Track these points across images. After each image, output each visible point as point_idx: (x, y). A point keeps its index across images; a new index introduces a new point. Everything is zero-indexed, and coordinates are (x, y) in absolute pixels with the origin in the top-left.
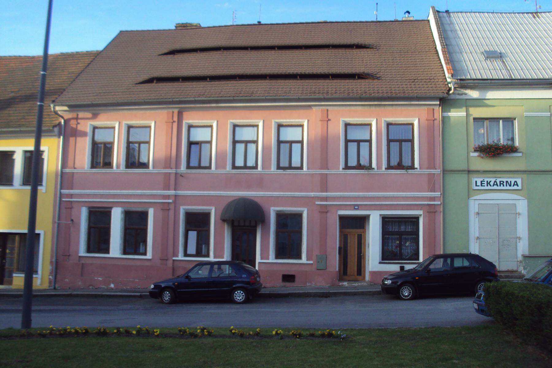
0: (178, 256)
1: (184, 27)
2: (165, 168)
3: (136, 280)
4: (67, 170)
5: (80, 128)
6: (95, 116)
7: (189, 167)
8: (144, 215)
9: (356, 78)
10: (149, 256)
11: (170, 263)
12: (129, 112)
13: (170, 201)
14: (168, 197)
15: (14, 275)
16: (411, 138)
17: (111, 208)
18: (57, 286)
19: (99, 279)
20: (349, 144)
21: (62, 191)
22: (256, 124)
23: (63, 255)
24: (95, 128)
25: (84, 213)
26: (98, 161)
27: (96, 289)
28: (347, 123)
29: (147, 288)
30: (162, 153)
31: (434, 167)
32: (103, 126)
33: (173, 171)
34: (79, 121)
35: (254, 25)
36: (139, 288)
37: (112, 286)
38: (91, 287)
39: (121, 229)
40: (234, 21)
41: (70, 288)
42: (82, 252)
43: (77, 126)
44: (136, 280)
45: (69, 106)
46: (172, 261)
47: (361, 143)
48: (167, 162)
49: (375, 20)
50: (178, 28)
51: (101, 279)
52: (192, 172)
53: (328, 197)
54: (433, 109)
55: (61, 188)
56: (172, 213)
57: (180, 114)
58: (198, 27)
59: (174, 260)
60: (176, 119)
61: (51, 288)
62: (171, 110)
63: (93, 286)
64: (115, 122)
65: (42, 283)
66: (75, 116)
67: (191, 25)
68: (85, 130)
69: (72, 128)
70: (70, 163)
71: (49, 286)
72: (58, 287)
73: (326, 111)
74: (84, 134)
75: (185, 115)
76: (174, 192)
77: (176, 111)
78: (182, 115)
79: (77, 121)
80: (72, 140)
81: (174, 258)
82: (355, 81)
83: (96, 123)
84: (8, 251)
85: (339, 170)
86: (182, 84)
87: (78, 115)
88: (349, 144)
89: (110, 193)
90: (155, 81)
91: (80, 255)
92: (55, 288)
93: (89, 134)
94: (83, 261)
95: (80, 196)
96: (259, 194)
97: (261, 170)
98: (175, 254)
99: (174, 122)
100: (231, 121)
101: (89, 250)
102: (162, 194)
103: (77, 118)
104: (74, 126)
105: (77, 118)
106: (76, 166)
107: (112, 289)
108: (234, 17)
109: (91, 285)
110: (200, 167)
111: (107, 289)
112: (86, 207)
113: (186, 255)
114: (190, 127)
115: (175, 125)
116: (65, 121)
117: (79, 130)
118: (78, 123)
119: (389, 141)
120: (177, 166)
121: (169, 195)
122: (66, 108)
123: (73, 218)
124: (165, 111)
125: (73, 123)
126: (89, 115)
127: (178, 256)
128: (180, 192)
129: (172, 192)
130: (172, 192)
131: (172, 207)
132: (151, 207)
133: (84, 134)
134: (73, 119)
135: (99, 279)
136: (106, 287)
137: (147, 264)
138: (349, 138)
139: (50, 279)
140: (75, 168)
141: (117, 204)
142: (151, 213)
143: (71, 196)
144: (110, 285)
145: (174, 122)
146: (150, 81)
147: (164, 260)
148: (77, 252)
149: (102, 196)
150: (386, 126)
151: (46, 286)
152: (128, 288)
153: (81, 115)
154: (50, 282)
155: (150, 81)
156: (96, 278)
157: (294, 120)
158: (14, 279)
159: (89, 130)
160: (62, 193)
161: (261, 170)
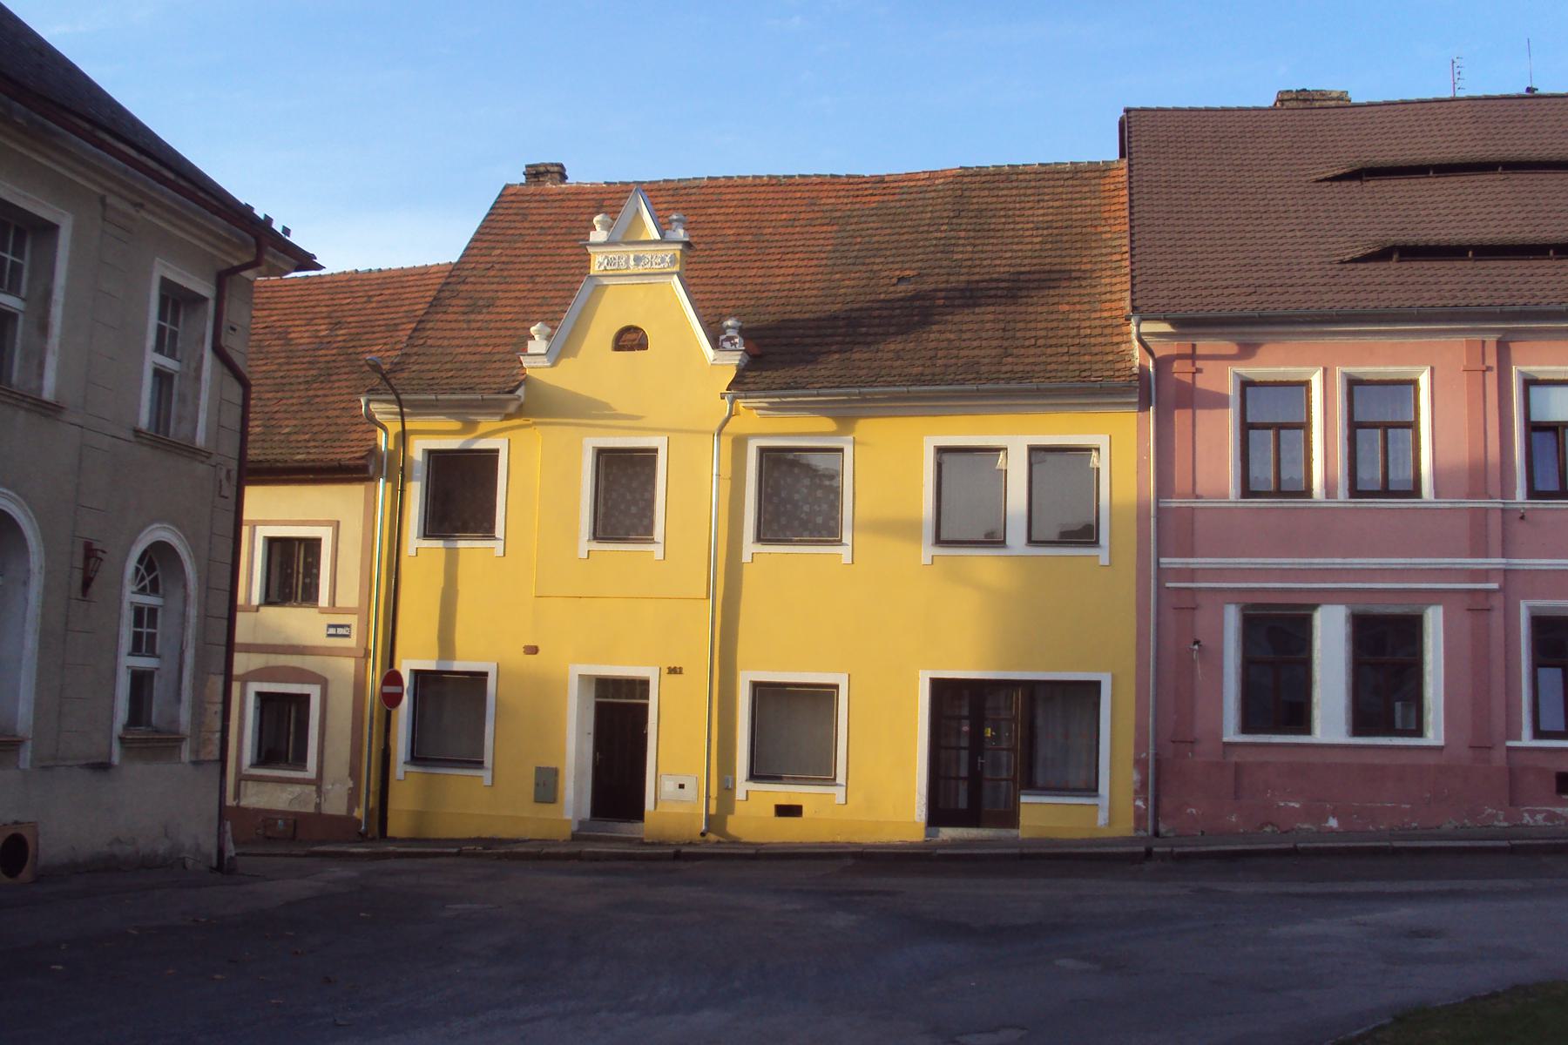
0: (1519, 738)
1: (1305, 100)
2: (1472, 495)
3: (1403, 806)
4: (1174, 503)
5: (1202, 382)
6: (1247, 351)
7: (1532, 493)
8: (1411, 628)
9: (1467, 255)
10: (1434, 734)
11: (1499, 758)
12: (1352, 341)
13: (1494, 586)
14: (1485, 575)
15: (1023, 799)
16: (1305, 420)
17: (1315, 607)
18: (1163, 829)
19: (1292, 804)
20: (1253, 434)
21: (1163, 560)
22: (1304, 378)
23: (1174, 742)
24: (1246, 384)
25: (1232, 619)
26: (389, 485)
27: (1286, 832)
28: (1529, 378)
29: (1438, 828)
30: (1461, 453)
31: (1486, 493)
32: (1375, 378)
33: (1496, 503)
34: (1199, 364)
35: (1520, 97)
36: (1415, 828)
37: (1333, 823)
38: (1268, 829)
39: (1346, 665)
40: (1457, 87)
41: (1203, 833)
42: (1231, 732)
43: (1194, 378)
44: (1403, 806)
45: (1174, 322)
46: (1504, 752)
47: (1283, 432)
48: (1478, 479)
49: (1449, 95)
50: (1287, 103)
51: (1297, 806)
52: (1550, 506)
53: (1510, 570)
54: (1484, 342)
55: (1159, 555)
56: (1497, 618)
57: (1503, 348)
58: (1341, 103)
59: (1510, 749)
60: (1492, 361)
61: (1142, 833)
62: (1477, 338)
63: (1272, 825)
64: (1416, 369)
65: (1111, 820)
66: (1189, 351)
67: (1323, 95)
68: (1225, 392)
69: (1179, 382)
70: (1180, 479)
71: (1137, 829)
72: (1167, 832)
73: (1480, 345)
74: (1220, 401)
75: (1517, 350)
76: (1504, 561)
77: (1491, 340)
78: (1508, 349)
79: (1194, 365)
80: (1181, 417)
81: (1510, 743)
82: (1546, 263)
83: (1256, 370)
84: (989, 732)
85: (1515, 499)
86: (1558, 263)
87: (1194, 346)
88: (1253, 434)
89: (1187, 564)
90: (1395, 257)
91: (1225, 739)
92: (1156, 834)
93: (1231, 400)
94: (1235, 758)
95: (1220, 573)
96: (1534, 565)
97: (1433, 499)
98: (1513, 732)
99: (1489, 369)
100: (1525, 369)
101: (1246, 728)
102: (1466, 566)
103: (1193, 357)
104: (1188, 378)
105: (1193, 357)
106: (1199, 490)
107: (1332, 830)
108: (1457, 76)
109: (1266, 824)
110: (1386, 492)
111: (1319, 832)
112: (1236, 603)
113: (1538, 733)
114: (1529, 383)
115: (1492, 379)
116: (1157, 362)
117: (1200, 389)
118: (1199, 371)
119: (1354, 426)
120: (1506, 490)
121: (1487, 571)
122: (1165, 327)
123: (1198, 638)
124: (1461, 340)
125: (1180, 370)
126: (1228, 347)
127: (1519, 738)
128: (1518, 563)
129: (1497, 562)
130: (1497, 562)
131: (1497, 602)
132: (1437, 604)
133: (1220, 401)
134: (1180, 357)
135: (1292, 804)
136: (1314, 829)
137: (1431, 759)
138: (1358, 418)
139: (1137, 808)
140: (1197, 497)
141: (1333, 596)
142: (1434, 622)
143: (1192, 574)
144: (1327, 821)
145: (1489, 369)
146: (1383, 254)
147: (1482, 747)
148: (1218, 732)
149: (1285, 574)
150: (1239, 388)
151: (1126, 827)
152: (1382, 827)
153: (1205, 346)
154: (1139, 817)
155: (1383, 254)
156: (1282, 804)
157: (1382, 369)
158: (1023, 811)
159: (1232, 390)
160: (1162, 566)
161: (1433, 499)
